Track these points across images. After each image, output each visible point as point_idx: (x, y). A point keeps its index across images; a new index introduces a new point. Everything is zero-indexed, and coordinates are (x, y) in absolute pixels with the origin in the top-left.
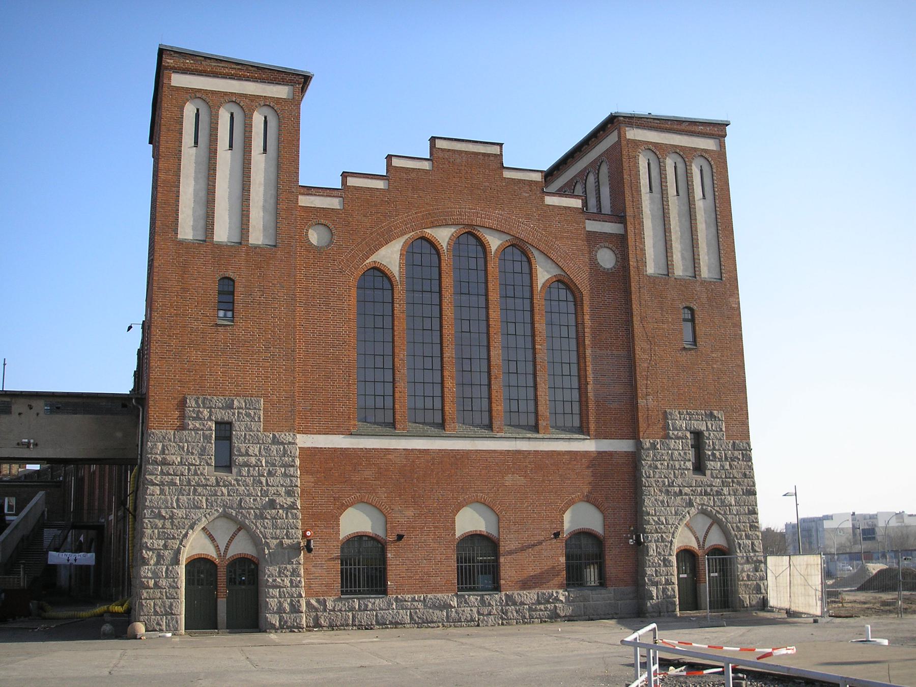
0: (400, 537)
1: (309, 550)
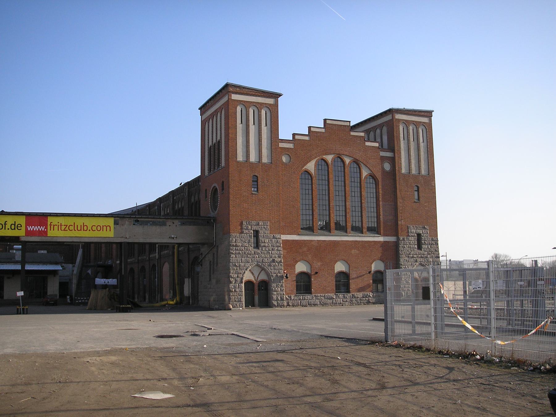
0: (316, 273)
1: (287, 277)
